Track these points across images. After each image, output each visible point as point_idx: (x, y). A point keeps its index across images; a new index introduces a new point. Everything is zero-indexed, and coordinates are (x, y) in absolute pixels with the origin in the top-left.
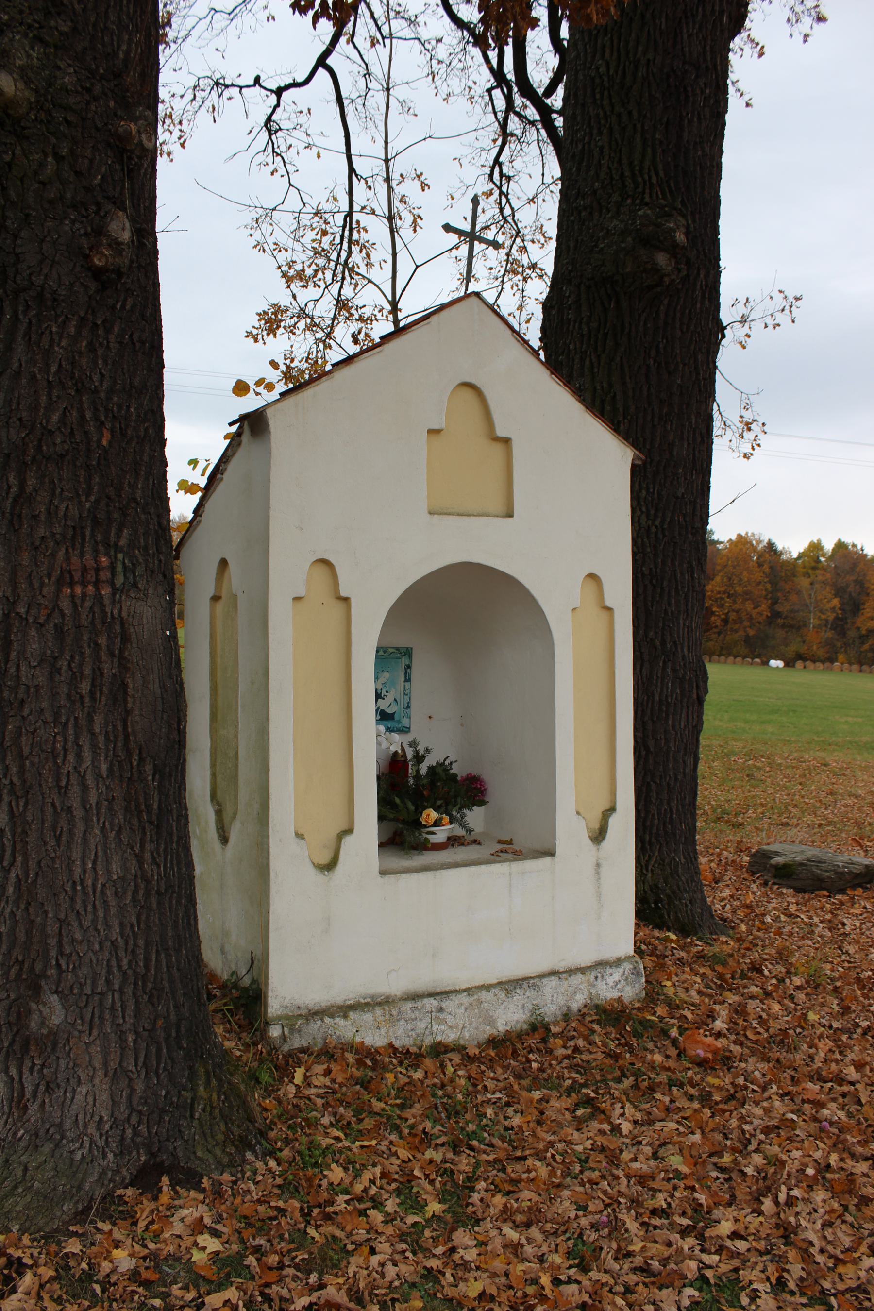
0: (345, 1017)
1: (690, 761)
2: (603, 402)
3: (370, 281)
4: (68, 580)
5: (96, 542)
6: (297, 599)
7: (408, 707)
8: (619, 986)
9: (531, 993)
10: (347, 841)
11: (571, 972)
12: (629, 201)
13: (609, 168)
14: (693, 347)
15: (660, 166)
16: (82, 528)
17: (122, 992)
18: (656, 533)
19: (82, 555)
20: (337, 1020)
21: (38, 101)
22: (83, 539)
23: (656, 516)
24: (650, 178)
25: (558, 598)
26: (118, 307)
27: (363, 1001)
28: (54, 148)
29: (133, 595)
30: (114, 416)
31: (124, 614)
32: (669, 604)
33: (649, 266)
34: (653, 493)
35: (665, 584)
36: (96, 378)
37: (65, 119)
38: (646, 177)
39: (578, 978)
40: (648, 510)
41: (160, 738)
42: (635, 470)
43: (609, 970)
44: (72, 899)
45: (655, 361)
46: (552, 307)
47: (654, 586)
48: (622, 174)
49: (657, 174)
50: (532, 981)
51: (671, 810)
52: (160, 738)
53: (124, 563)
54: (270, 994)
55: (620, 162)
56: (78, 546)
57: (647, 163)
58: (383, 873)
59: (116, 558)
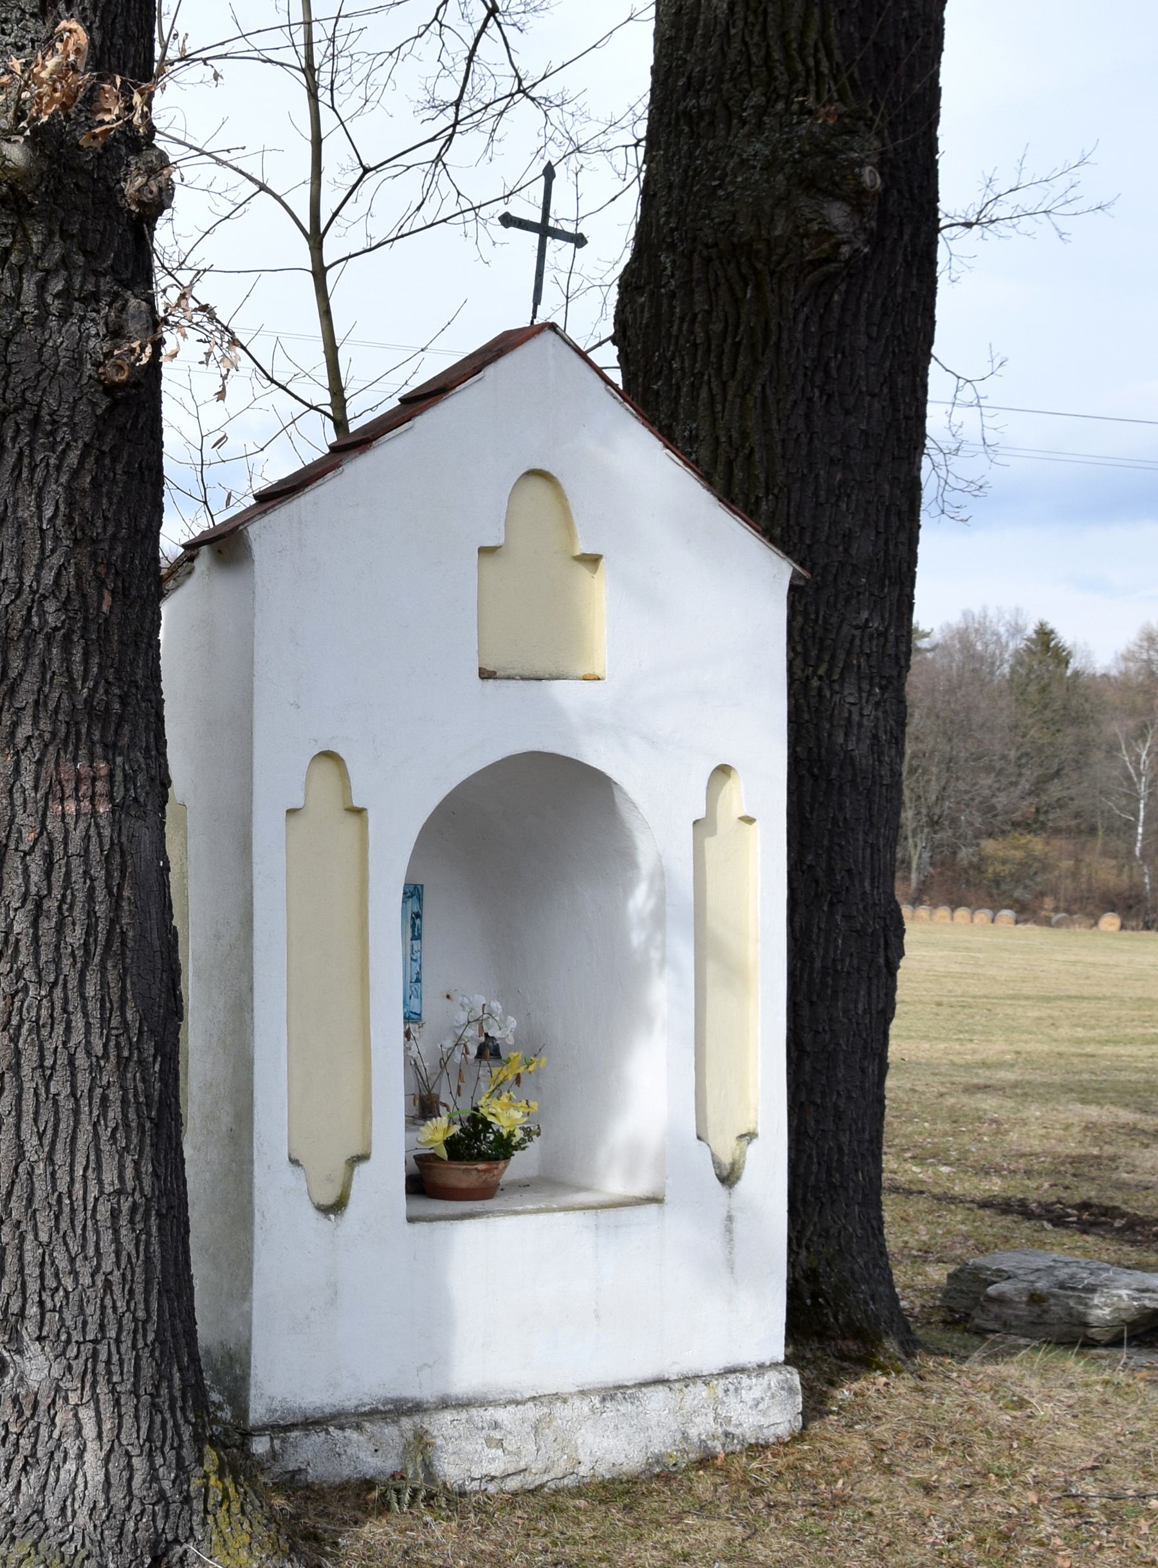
0: (358, 1427)
1: (872, 1068)
2: (730, 464)
3: (263, 188)
4: (59, 794)
5: (93, 743)
6: (291, 812)
7: (418, 980)
8: (761, 1407)
9: (626, 1408)
10: (362, 1169)
11: (688, 1380)
12: (780, 106)
13: (745, 43)
14: (888, 364)
15: (836, 43)
16: (77, 723)
17: (118, 1341)
18: (820, 689)
19: (75, 760)
20: (348, 1432)
21: (50, 170)
22: (78, 739)
23: (819, 658)
24: (818, 63)
25: (657, 801)
26: (129, 426)
27: (381, 1408)
28: (61, 226)
29: (133, 813)
30: (117, 571)
31: (124, 839)
32: (841, 808)
33: (815, 227)
34: (816, 621)
35: (834, 773)
36: (99, 523)
37: (76, 184)
38: (811, 62)
39: (700, 1391)
40: (806, 650)
41: (160, 1006)
42: (795, 592)
43: (745, 1381)
44: (57, 1218)
45: (822, 391)
46: (639, 289)
47: (816, 778)
48: (768, 55)
49: (829, 56)
50: (629, 1391)
51: (840, 1150)
52: (160, 1006)
53: (124, 770)
54: (253, 1392)
55: (764, 32)
56: (71, 748)
57: (813, 36)
58: (411, 1220)
59: (114, 763)
